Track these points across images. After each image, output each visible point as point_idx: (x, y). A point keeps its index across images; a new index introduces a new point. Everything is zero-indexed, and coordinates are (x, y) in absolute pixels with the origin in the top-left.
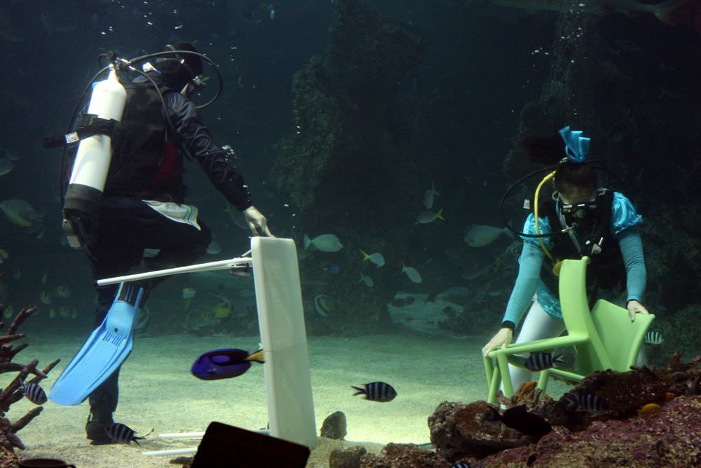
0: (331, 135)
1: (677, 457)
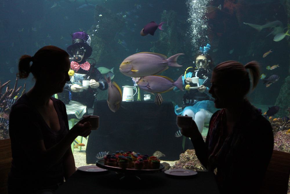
0: (100, 51)
1: (286, 150)
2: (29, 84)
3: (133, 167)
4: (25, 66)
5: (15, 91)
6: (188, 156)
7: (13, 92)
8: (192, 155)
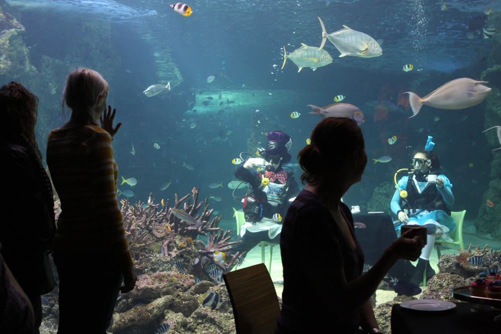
6: (440, 282)
7: (193, 210)
8: (445, 280)
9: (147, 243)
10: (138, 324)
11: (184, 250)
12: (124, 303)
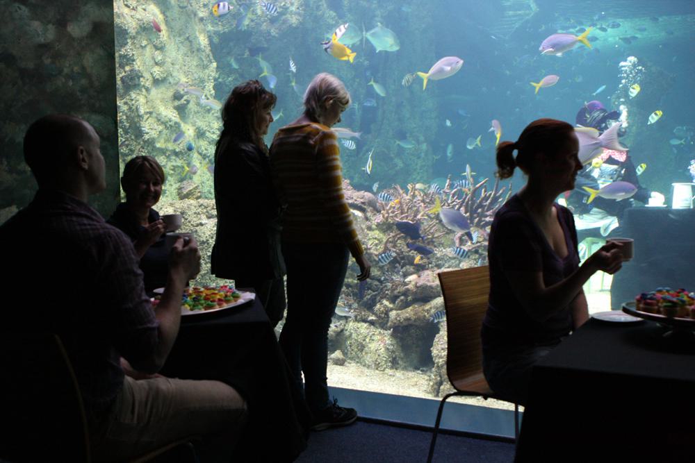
2: (518, 181)
3: (688, 315)
4: (505, 159)
5: (495, 194)
9: (436, 235)
10: (414, 323)
11: (479, 244)
12: (402, 300)
